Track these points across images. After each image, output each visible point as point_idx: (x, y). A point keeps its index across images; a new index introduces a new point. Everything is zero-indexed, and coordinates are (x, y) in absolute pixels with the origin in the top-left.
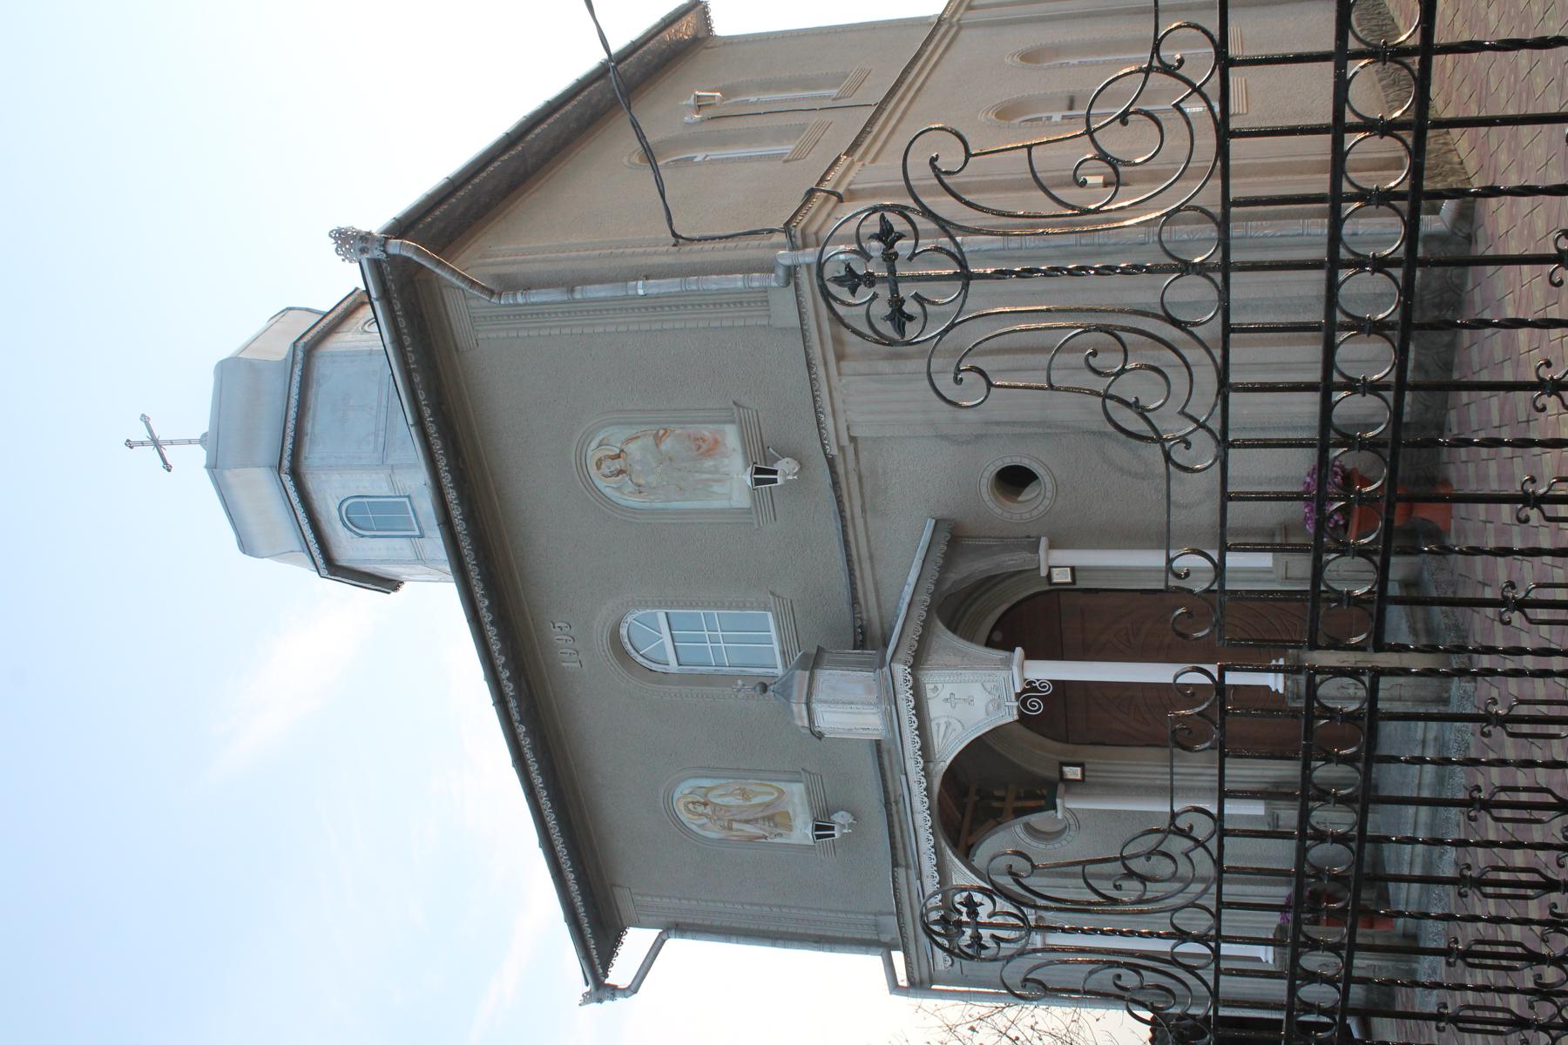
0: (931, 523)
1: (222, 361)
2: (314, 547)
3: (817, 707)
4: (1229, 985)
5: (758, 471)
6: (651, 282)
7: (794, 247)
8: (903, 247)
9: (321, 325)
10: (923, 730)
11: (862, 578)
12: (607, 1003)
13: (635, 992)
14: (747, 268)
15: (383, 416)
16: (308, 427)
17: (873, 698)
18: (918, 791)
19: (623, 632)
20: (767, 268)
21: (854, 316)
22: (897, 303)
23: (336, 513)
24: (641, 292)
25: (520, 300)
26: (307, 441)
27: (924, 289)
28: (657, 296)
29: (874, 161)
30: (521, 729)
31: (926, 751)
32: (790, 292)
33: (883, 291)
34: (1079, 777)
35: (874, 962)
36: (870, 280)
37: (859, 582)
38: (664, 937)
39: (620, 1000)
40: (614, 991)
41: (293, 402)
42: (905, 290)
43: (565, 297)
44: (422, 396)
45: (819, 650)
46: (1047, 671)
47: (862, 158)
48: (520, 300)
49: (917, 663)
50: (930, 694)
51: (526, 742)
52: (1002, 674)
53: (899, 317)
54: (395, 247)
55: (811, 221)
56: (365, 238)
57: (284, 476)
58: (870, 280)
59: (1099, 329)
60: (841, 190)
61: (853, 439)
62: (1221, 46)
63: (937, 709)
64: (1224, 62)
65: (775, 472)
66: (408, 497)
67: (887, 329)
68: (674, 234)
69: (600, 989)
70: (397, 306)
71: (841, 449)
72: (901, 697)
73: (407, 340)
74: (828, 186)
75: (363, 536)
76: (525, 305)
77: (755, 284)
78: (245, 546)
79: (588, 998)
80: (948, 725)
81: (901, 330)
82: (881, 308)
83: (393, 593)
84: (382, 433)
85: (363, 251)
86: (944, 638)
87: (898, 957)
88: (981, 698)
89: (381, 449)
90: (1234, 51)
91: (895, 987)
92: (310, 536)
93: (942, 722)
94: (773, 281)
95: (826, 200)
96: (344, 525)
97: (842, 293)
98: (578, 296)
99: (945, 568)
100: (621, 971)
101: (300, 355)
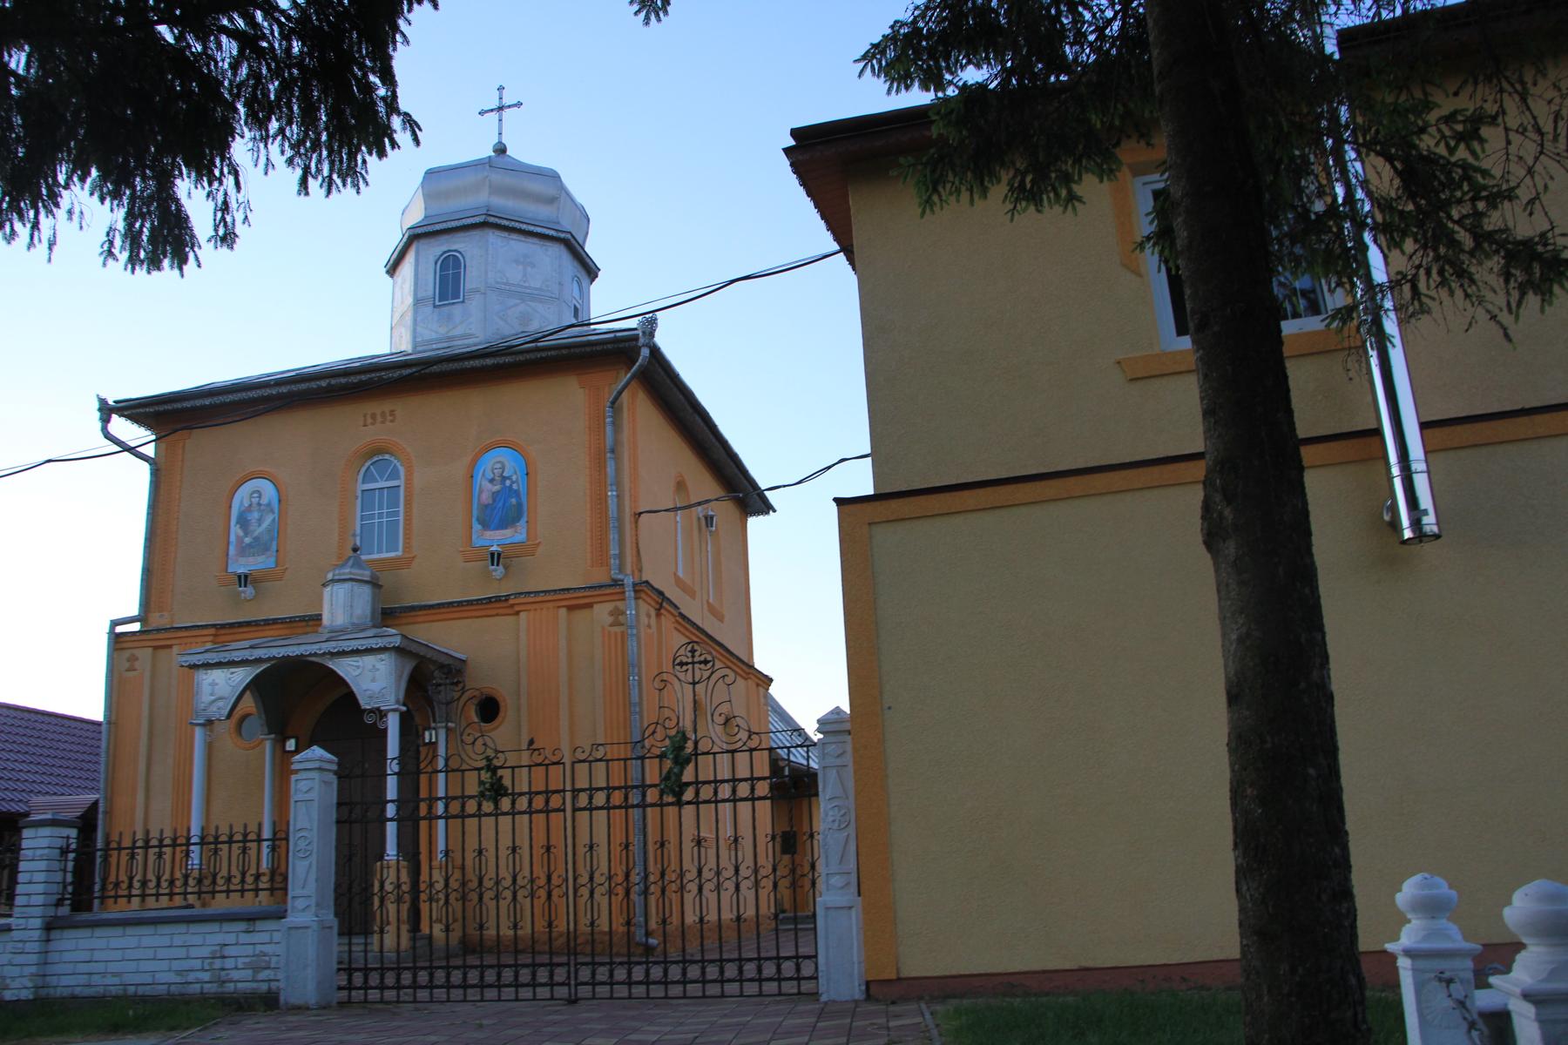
0: (463, 657)
1: (559, 177)
2: (430, 229)
3: (347, 585)
4: (115, 853)
5: (499, 555)
6: (615, 500)
7: (635, 585)
8: (702, 666)
9: (576, 245)
10: (356, 652)
11: (440, 613)
12: (98, 414)
13: (106, 437)
14: (621, 556)
15: (519, 289)
16: (514, 236)
17: (355, 621)
18: (314, 648)
19: (387, 457)
20: (621, 569)
21: (682, 651)
22: (687, 664)
23: (453, 248)
24: (609, 493)
25: (608, 420)
26: (506, 234)
27: (690, 672)
28: (606, 501)
29: (676, 628)
30: (324, 383)
31: (343, 654)
32: (607, 581)
33: (690, 660)
34: (288, 749)
35: (134, 610)
36: (693, 657)
37: (425, 612)
38: (151, 461)
39: (99, 425)
40: (106, 420)
41: (531, 228)
42: (690, 666)
43: (608, 447)
44: (553, 353)
45: (381, 586)
46: (393, 725)
47: (677, 622)
48: (608, 420)
49: (399, 650)
50: (379, 656)
51: (314, 385)
52: (392, 699)
53: (682, 664)
54: (645, 352)
55: (647, 594)
56: (652, 335)
57: (484, 217)
58: (693, 657)
59: (712, 715)
60: (662, 611)
61: (517, 613)
62: (755, 749)
63: (369, 660)
64: (751, 750)
65: (498, 565)
66: (463, 302)
67: (678, 661)
68: (641, 513)
69: (107, 411)
70: (609, 346)
71: (512, 606)
72: (379, 640)
73: (588, 349)
74: (664, 604)
75: (436, 263)
76: (604, 423)
77: (612, 561)
78: (430, 173)
79: (103, 402)
80: (358, 667)
81: (678, 664)
82: (685, 660)
83: (385, 270)
84: (508, 288)
85: (644, 333)
86: (409, 667)
87: (136, 627)
88: (375, 687)
89: (498, 286)
90: (754, 753)
91: (115, 623)
92: (438, 227)
93: (360, 664)
94: (615, 574)
95: (657, 602)
96: (445, 252)
97: (689, 648)
98: (609, 455)
99: (442, 666)
100: (123, 428)
101: (562, 235)
